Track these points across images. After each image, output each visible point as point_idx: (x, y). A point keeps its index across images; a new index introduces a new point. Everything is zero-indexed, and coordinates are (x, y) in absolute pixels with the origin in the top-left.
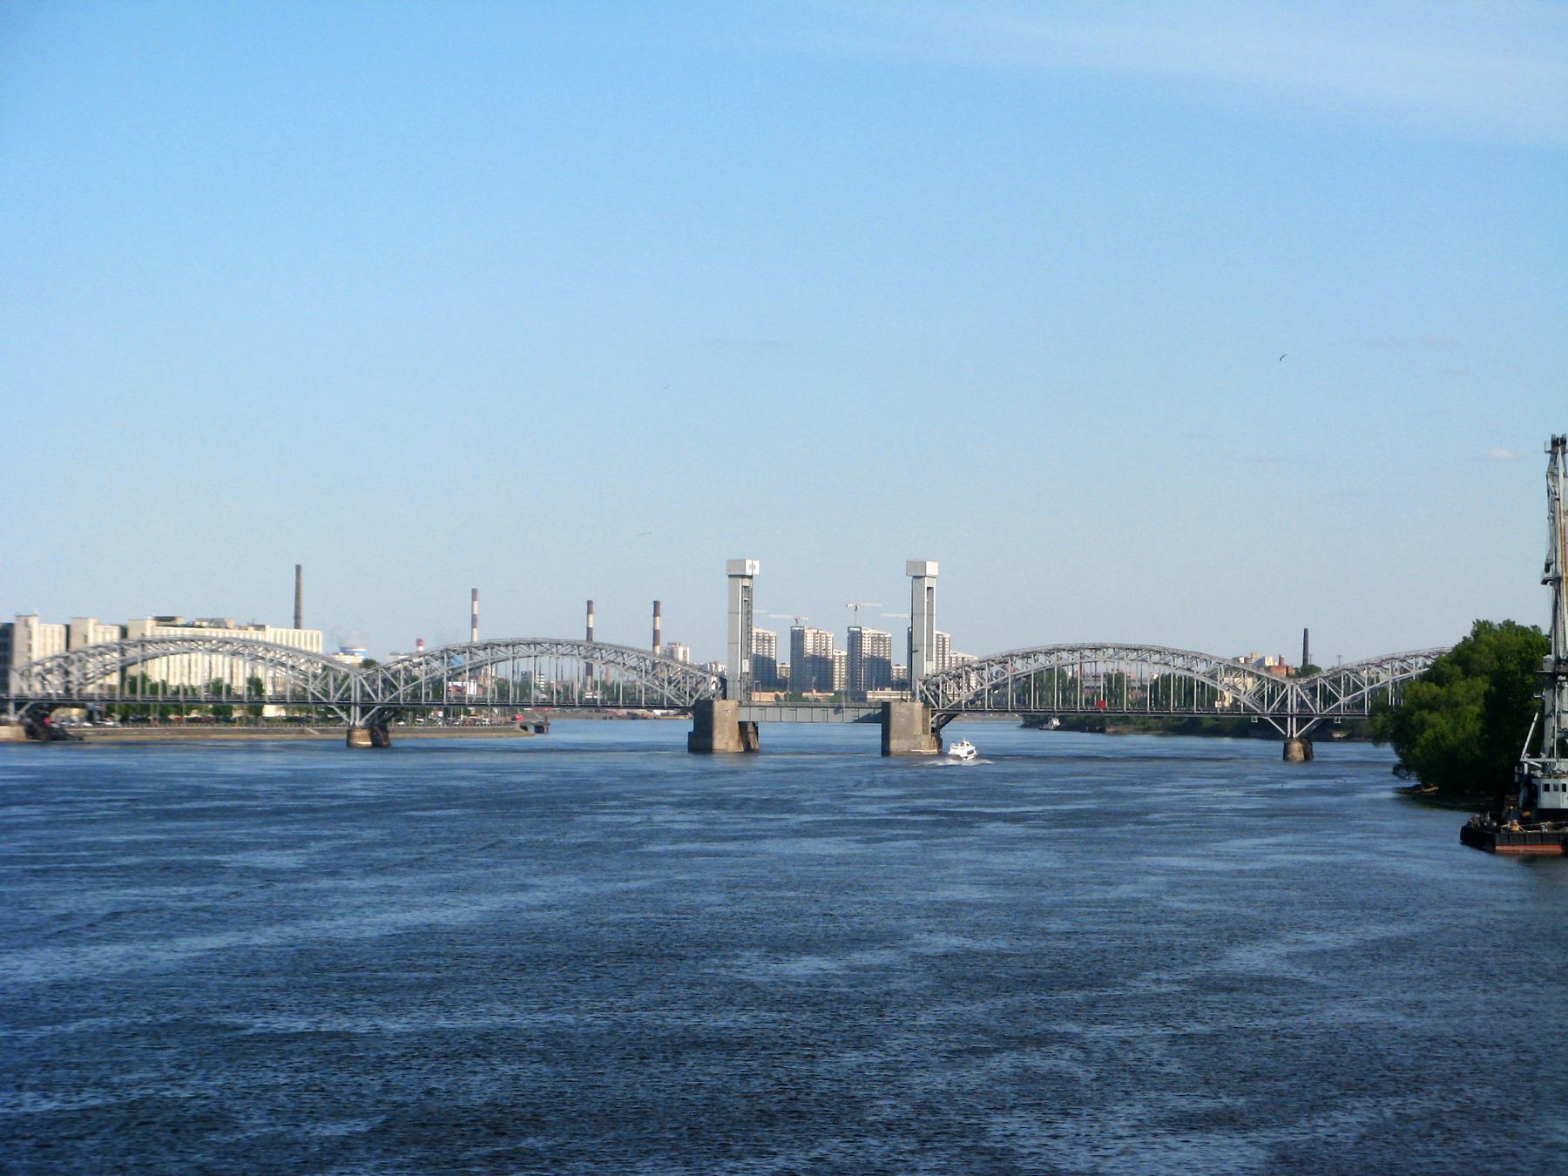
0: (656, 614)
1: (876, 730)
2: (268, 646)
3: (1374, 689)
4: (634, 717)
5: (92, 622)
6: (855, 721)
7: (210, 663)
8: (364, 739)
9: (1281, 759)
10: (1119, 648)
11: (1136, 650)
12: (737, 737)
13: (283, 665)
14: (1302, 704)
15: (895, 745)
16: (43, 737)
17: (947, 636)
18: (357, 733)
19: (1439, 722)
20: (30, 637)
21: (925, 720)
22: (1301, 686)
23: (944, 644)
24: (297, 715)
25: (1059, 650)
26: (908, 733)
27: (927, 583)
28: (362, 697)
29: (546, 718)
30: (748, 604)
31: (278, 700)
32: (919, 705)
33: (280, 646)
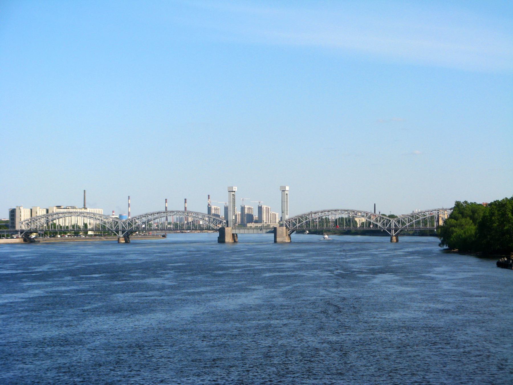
0: (185, 202)
1: (273, 235)
2: (87, 213)
3: (416, 221)
4: (182, 232)
5: (38, 208)
6: (266, 233)
7: (77, 219)
8: (122, 240)
9: (390, 242)
10: (342, 210)
11: (347, 211)
12: (232, 238)
13: (99, 219)
14: (395, 226)
15: (278, 239)
16: (28, 242)
17: (269, 207)
18: (121, 239)
19: (458, 231)
20: (21, 212)
21: (286, 232)
22: (395, 221)
23: (268, 210)
24: (97, 234)
25: (325, 211)
26: (282, 236)
27: (286, 192)
28: (122, 228)
29: (166, 233)
30: (234, 199)
31: (92, 230)
32: (285, 228)
33: (91, 213)
